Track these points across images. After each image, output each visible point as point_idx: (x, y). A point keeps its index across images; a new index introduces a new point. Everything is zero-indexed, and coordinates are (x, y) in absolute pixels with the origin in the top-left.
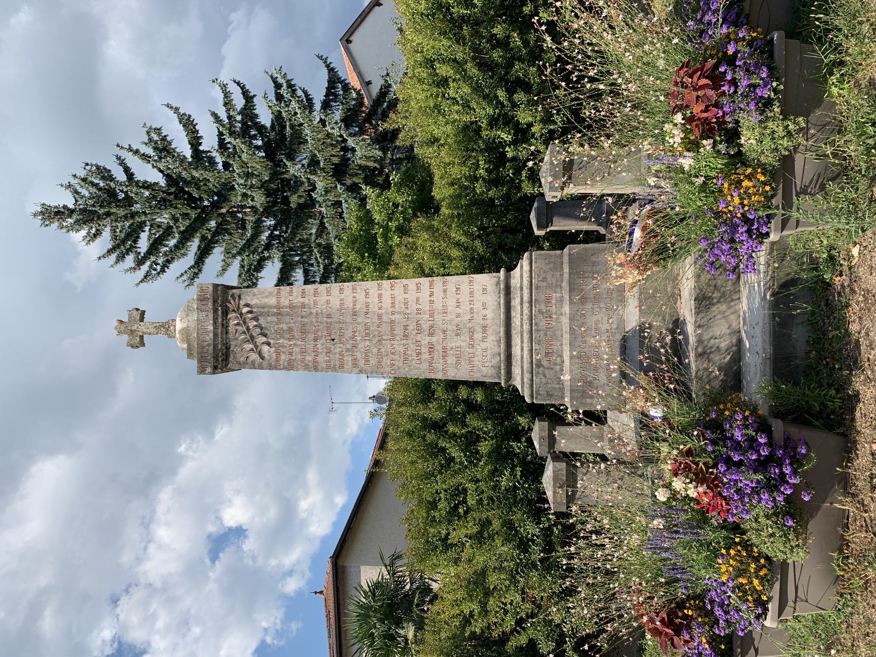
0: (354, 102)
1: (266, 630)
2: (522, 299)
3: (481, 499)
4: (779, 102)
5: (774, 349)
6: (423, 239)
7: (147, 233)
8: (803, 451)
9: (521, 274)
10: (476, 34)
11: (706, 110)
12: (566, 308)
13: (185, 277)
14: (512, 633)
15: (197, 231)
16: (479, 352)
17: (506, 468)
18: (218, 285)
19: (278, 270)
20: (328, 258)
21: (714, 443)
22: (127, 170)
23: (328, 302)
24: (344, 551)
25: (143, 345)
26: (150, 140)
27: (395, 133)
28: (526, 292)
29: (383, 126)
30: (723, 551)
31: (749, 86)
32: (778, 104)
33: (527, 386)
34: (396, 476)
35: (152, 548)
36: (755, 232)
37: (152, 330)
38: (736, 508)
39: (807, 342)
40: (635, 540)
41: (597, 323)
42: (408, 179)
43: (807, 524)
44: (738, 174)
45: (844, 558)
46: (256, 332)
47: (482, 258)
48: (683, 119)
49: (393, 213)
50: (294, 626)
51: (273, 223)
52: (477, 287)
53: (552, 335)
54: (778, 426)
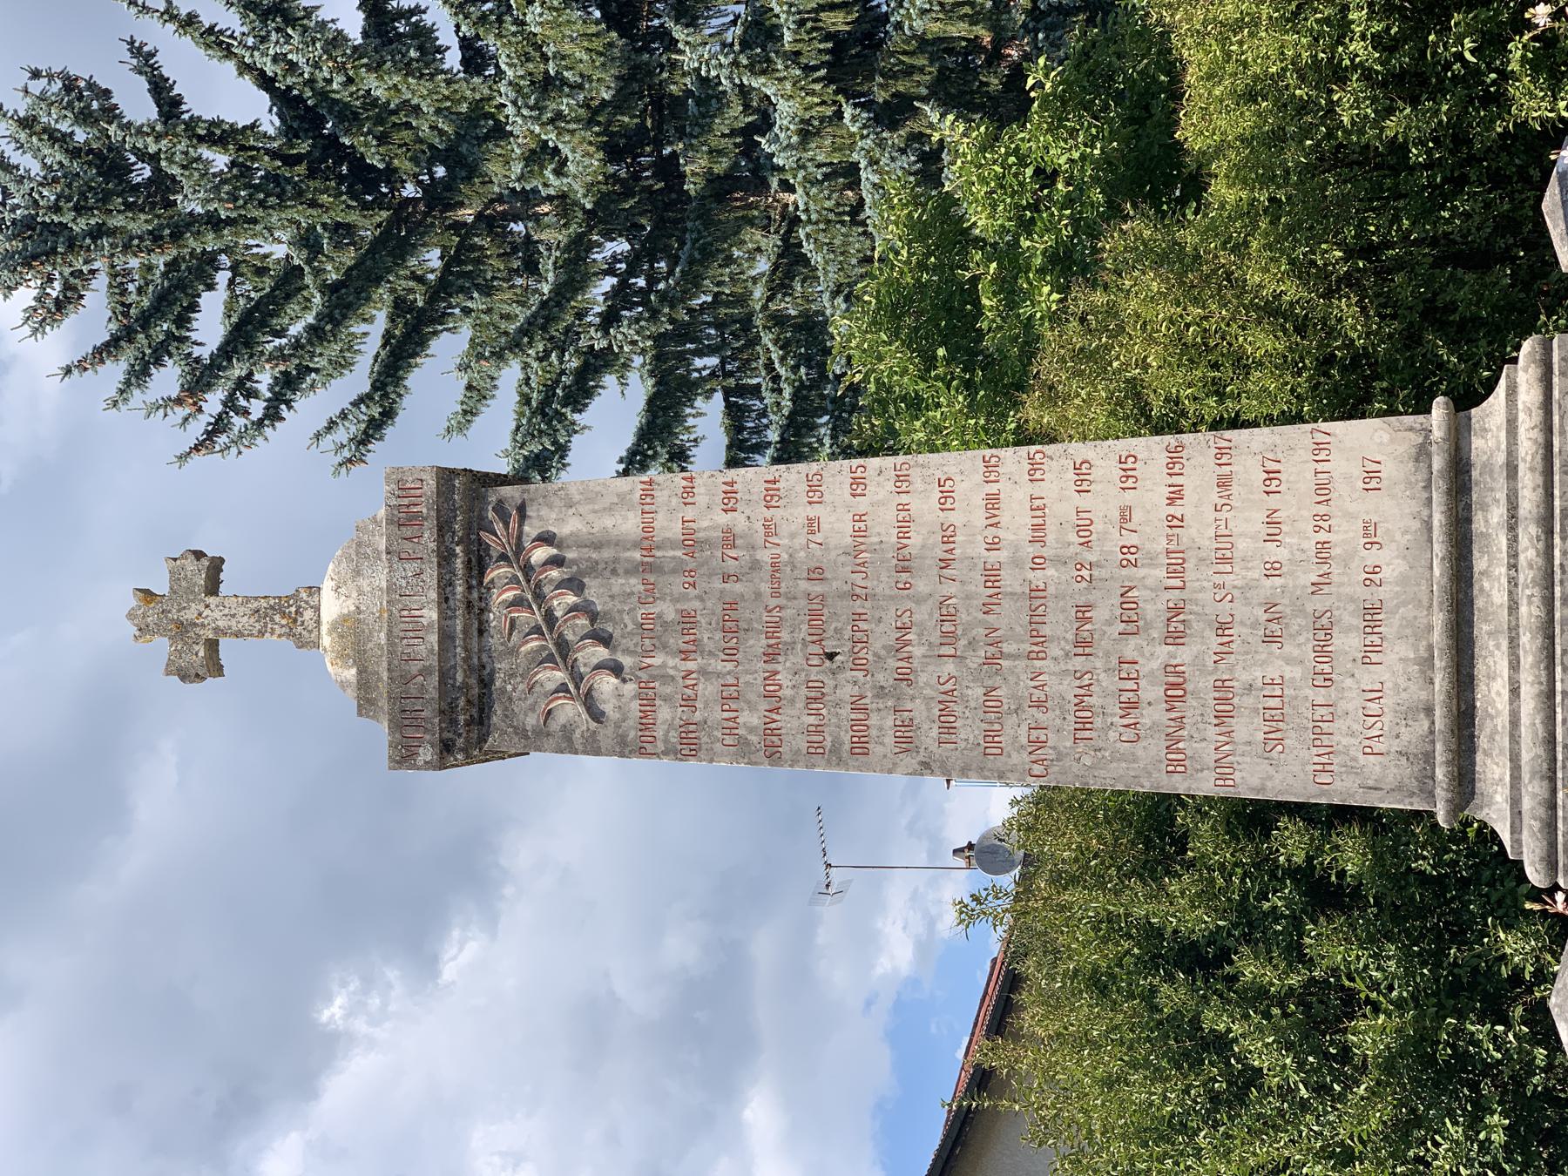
2: (1513, 507)
6: (1144, 295)
9: (1508, 417)
13: (342, 434)
15: (378, 281)
16: (1352, 703)
18: (453, 473)
20: (807, 360)
22: (160, 88)
23: (812, 525)
25: (216, 669)
28: (1529, 484)
34: (1049, 1128)
42: (1089, 84)
47: (1357, 358)
52: (1344, 467)
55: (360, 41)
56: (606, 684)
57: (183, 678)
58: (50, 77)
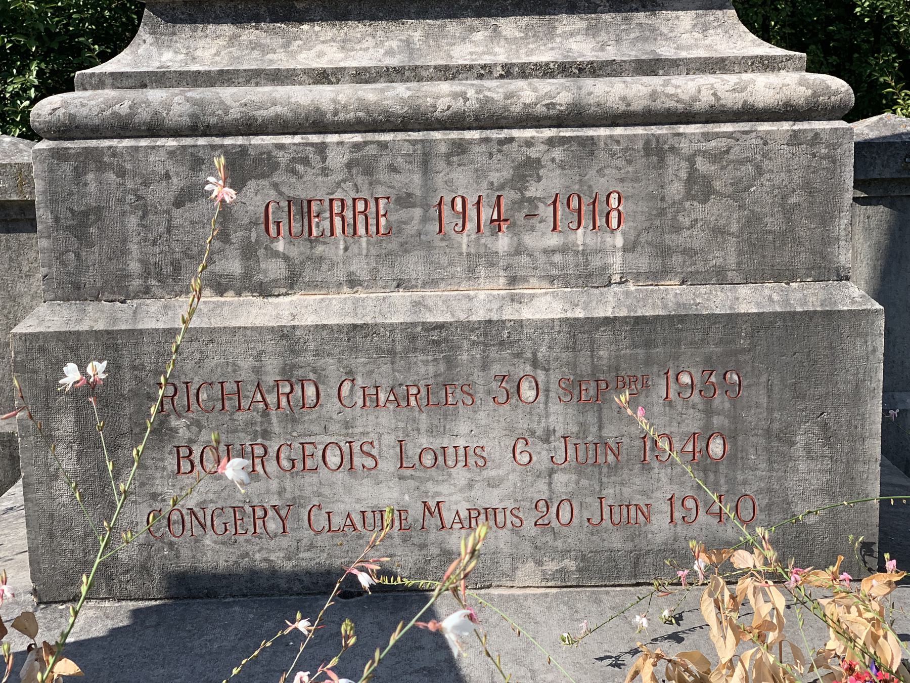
12: (545, 305)
28: (634, 91)
53: (404, 235)
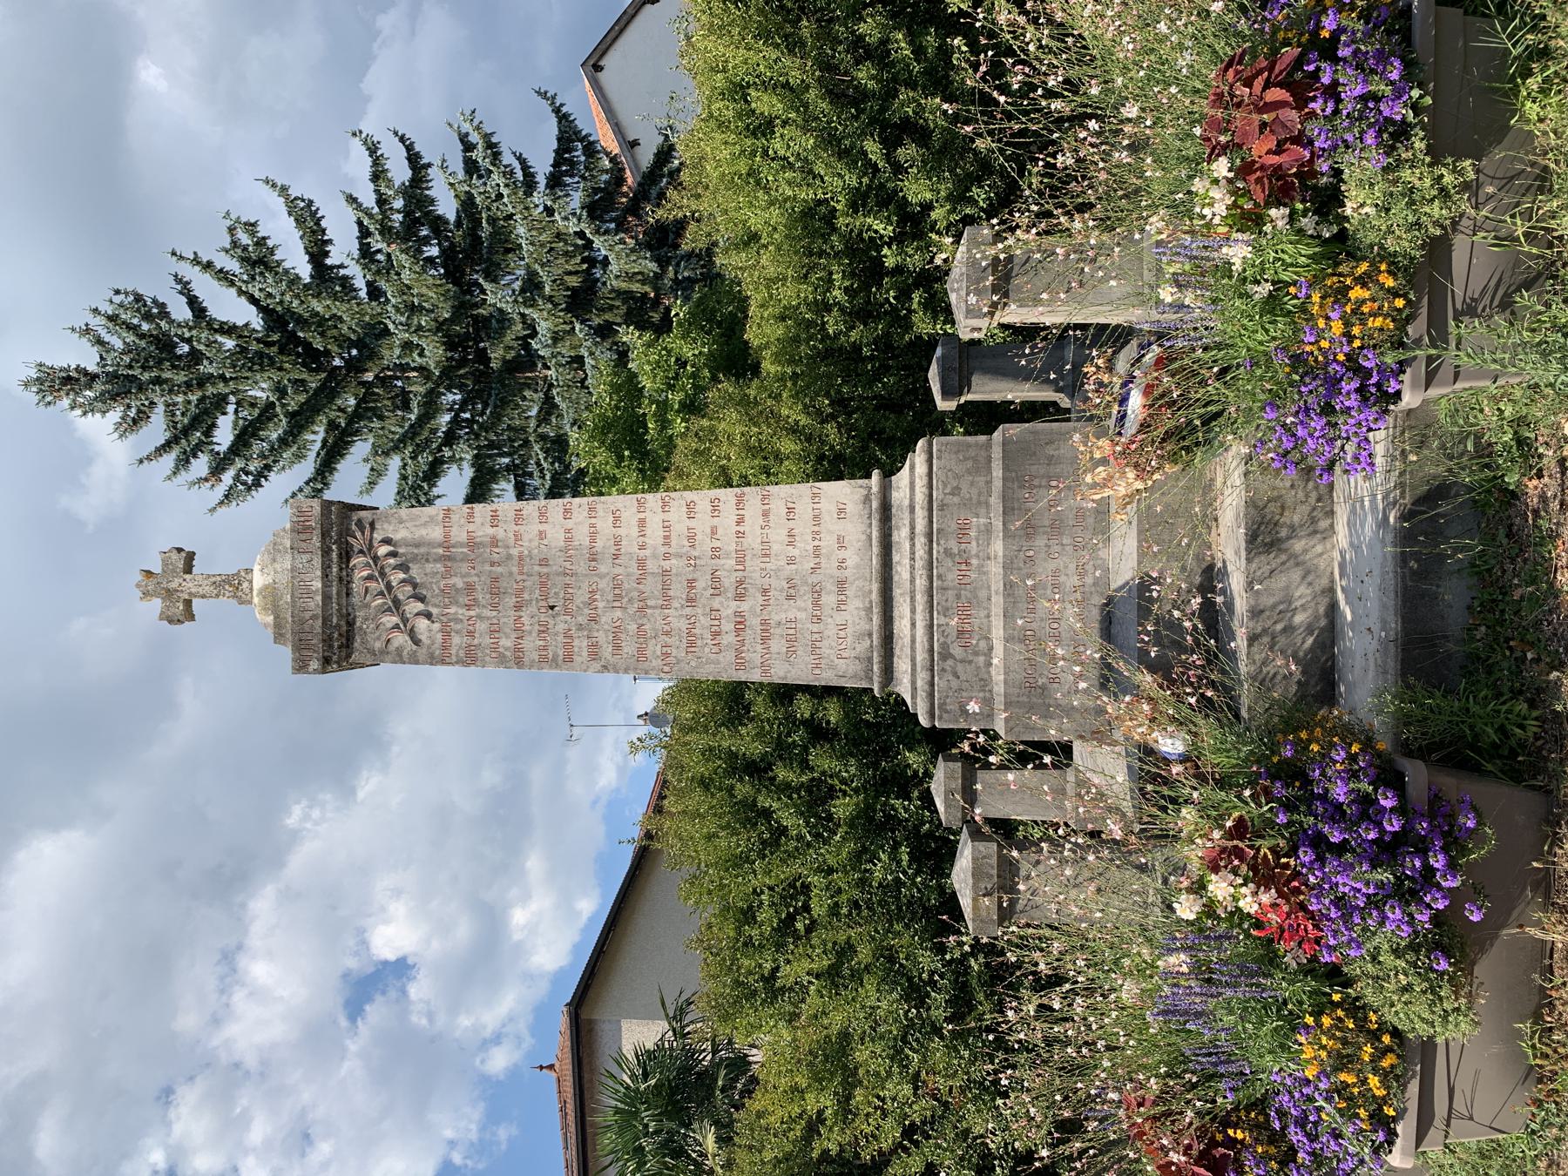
0: (605, 177)
1: (452, 1144)
2: (913, 528)
3: (836, 904)
4: (1423, 129)
5: (1404, 628)
6: (730, 423)
7: (231, 417)
8: (1470, 824)
10: (825, 34)
11: (1279, 150)
12: (998, 547)
14: (893, 1151)
16: (831, 631)
17: (882, 847)
19: (467, 482)
20: (560, 460)
21: (1289, 806)
22: (193, 302)
23: (542, 535)
24: (591, 993)
25: (192, 617)
26: (235, 244)
27: (680, 225)
28: (921, 514)
29: (656, 215)
30: (1309, 1020)
31: (1364, 98)
32: (1422, 134)
33: (922, 695)
35: (239, 997)
36: (1373, 390)
37: (207, 589)
38: (1335, 933)
39: (1469, 607)
40: (1129, 991)
41: (1056, 573)
42: (703, 317)
43: (1473, 963)
44: (1340, 275)
45: (1543, 1030)
46: (404, 592)
48: (1230, 170)
49: (676, 378)
50: (503, 1133)
51: (458, 397)
53: (969, 599)
54: (1416, 774)
55: (308, 280)
56: (422, 624)
57: (170, 622)
58: (126, 293)
